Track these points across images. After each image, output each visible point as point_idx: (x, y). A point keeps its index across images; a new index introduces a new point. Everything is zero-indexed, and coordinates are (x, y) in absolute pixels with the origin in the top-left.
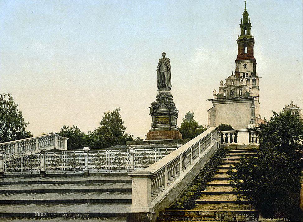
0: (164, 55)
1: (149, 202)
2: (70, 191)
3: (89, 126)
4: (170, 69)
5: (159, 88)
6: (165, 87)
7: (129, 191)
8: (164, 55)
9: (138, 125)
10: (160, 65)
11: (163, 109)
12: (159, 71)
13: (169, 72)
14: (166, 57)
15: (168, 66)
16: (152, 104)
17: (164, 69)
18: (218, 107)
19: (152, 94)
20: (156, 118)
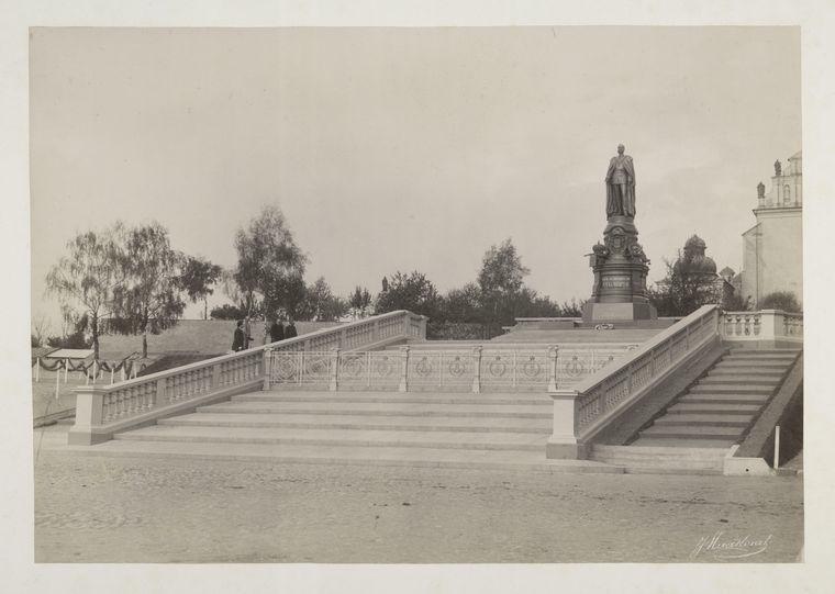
0: (621, 150)
1: (576, 431)
2: (715, 402)
3: (454, 276)
4: (633, 179)
5: (609, 215)
6: (622, 214)
7: (550, 417)
8: (621, 150)
9: (561, 276)
10: (612, 171)
11: (618, 255)
12: (610, 181)
13: (631, 184)
14: (625, 153)
15: (629, 174)
16: (595, 249)
17: (620, 179)
18: (768, 221)
19: (594, 228)
20: (601, 277)
